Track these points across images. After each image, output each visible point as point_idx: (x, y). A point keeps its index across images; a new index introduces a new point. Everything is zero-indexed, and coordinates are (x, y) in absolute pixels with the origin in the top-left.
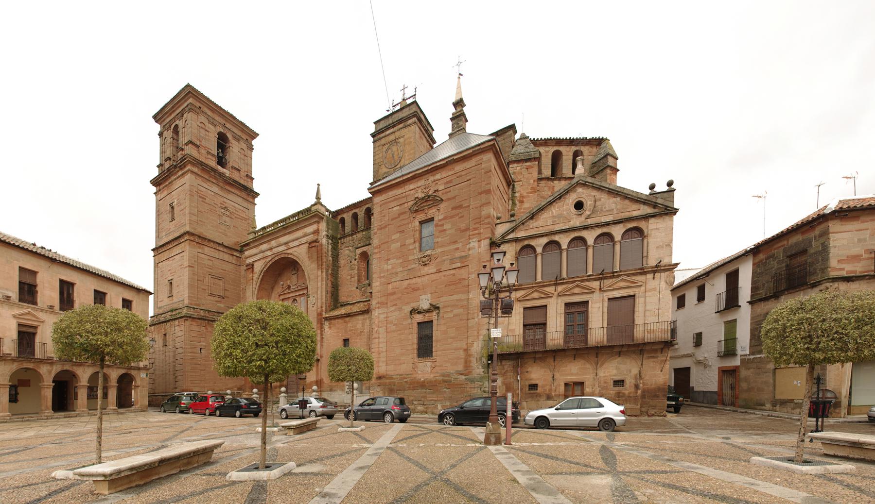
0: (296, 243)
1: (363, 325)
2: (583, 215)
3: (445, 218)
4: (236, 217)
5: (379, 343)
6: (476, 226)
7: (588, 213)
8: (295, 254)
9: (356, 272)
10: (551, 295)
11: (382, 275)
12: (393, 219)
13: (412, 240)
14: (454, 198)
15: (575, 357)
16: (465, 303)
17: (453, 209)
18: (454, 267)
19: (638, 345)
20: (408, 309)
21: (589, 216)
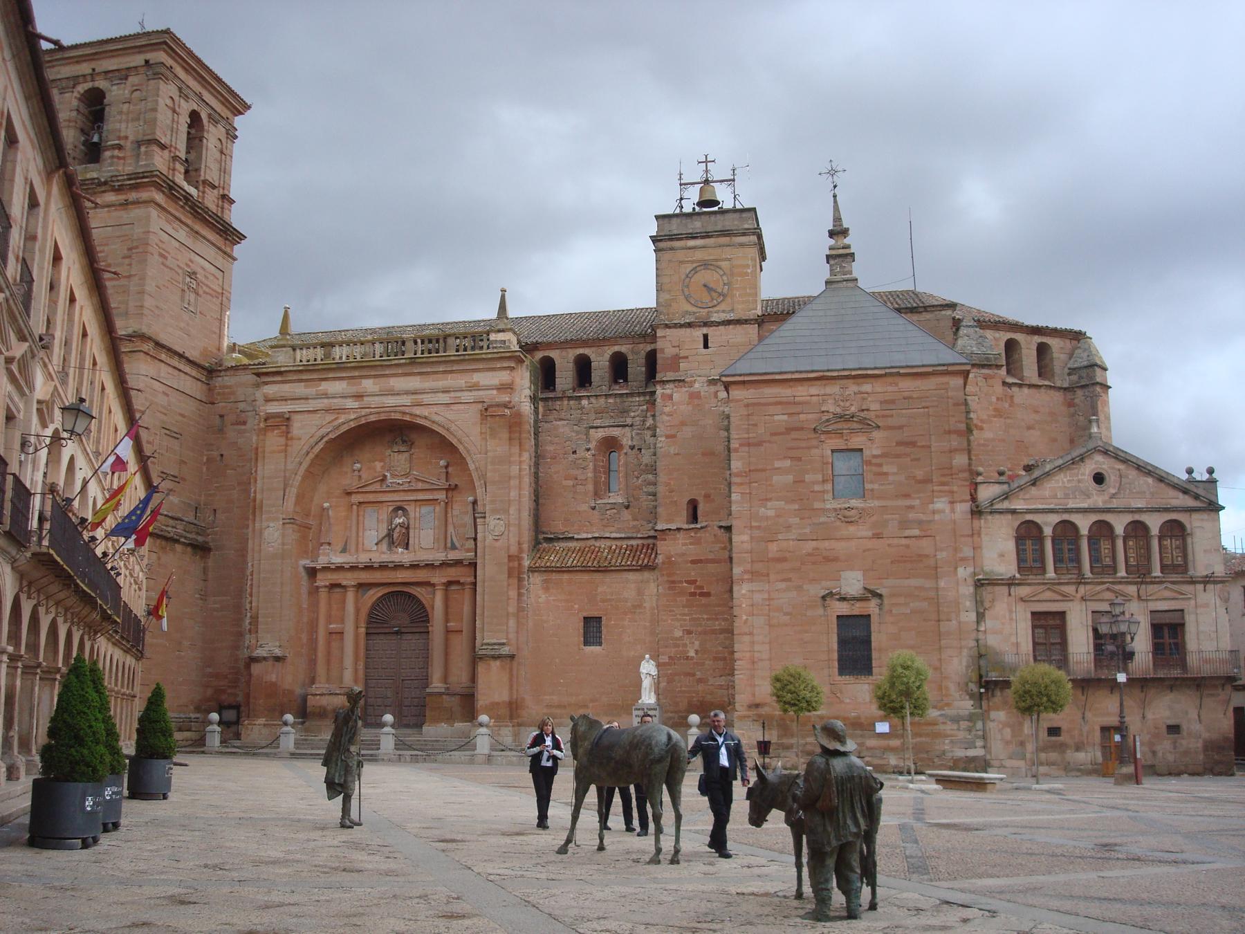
0: (444, 398)
1: (640, 592)
2: (1105, 493)
3: (883, 455)
4: (205, 292)
5: (753, 643)
6: (944, 479)
7: (1113, 491)
9: (590, 475)
10: (1072, 598)
11: (754, 524)
12: (773, 434)
13: (819, 477)
14: (901, 427)
15: (1112, 690)
16: (932, 594)
17: (899, 444)
18: (906, 535)
19: (1195, 679)
20: (818, 590)
21: (1114, 494)
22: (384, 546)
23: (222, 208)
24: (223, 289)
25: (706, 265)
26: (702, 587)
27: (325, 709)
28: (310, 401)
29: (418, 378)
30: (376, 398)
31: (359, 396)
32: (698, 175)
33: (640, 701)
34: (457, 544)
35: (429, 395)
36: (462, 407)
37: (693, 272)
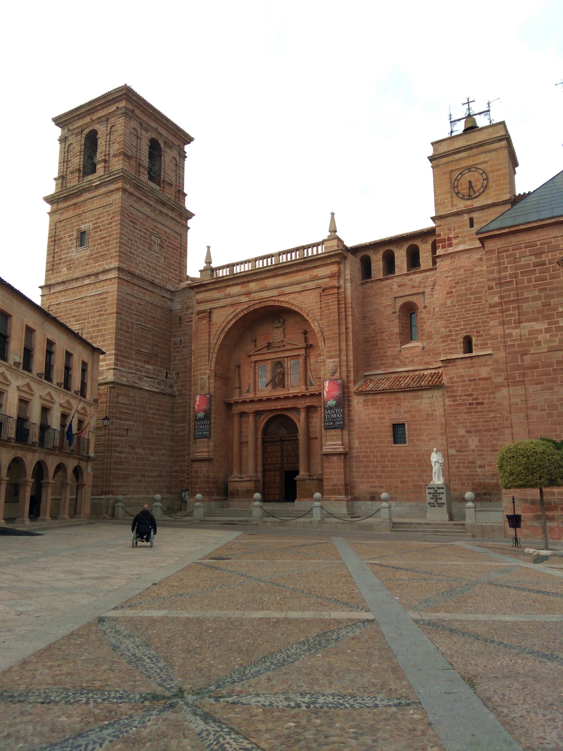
0: (297, 288)
4: (168, 246)
8: (292, 301)
22: (270, 387)
23: (179, 198)
24: (181, 245)
25: (469, 169)
26: (477, 399)
27: (238, 491)
28: (221, 301)
29: (281, 277)
30: (258, 294)
31: (248, 294)
32: (462, 113)
33: (431, 483)
34: (313, 382)
35: (289, 287)
36: (308, 292)
37: (460, 176)
